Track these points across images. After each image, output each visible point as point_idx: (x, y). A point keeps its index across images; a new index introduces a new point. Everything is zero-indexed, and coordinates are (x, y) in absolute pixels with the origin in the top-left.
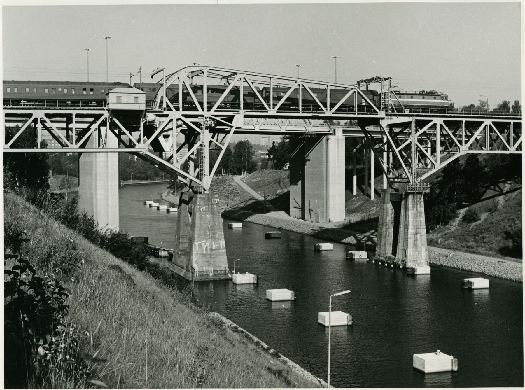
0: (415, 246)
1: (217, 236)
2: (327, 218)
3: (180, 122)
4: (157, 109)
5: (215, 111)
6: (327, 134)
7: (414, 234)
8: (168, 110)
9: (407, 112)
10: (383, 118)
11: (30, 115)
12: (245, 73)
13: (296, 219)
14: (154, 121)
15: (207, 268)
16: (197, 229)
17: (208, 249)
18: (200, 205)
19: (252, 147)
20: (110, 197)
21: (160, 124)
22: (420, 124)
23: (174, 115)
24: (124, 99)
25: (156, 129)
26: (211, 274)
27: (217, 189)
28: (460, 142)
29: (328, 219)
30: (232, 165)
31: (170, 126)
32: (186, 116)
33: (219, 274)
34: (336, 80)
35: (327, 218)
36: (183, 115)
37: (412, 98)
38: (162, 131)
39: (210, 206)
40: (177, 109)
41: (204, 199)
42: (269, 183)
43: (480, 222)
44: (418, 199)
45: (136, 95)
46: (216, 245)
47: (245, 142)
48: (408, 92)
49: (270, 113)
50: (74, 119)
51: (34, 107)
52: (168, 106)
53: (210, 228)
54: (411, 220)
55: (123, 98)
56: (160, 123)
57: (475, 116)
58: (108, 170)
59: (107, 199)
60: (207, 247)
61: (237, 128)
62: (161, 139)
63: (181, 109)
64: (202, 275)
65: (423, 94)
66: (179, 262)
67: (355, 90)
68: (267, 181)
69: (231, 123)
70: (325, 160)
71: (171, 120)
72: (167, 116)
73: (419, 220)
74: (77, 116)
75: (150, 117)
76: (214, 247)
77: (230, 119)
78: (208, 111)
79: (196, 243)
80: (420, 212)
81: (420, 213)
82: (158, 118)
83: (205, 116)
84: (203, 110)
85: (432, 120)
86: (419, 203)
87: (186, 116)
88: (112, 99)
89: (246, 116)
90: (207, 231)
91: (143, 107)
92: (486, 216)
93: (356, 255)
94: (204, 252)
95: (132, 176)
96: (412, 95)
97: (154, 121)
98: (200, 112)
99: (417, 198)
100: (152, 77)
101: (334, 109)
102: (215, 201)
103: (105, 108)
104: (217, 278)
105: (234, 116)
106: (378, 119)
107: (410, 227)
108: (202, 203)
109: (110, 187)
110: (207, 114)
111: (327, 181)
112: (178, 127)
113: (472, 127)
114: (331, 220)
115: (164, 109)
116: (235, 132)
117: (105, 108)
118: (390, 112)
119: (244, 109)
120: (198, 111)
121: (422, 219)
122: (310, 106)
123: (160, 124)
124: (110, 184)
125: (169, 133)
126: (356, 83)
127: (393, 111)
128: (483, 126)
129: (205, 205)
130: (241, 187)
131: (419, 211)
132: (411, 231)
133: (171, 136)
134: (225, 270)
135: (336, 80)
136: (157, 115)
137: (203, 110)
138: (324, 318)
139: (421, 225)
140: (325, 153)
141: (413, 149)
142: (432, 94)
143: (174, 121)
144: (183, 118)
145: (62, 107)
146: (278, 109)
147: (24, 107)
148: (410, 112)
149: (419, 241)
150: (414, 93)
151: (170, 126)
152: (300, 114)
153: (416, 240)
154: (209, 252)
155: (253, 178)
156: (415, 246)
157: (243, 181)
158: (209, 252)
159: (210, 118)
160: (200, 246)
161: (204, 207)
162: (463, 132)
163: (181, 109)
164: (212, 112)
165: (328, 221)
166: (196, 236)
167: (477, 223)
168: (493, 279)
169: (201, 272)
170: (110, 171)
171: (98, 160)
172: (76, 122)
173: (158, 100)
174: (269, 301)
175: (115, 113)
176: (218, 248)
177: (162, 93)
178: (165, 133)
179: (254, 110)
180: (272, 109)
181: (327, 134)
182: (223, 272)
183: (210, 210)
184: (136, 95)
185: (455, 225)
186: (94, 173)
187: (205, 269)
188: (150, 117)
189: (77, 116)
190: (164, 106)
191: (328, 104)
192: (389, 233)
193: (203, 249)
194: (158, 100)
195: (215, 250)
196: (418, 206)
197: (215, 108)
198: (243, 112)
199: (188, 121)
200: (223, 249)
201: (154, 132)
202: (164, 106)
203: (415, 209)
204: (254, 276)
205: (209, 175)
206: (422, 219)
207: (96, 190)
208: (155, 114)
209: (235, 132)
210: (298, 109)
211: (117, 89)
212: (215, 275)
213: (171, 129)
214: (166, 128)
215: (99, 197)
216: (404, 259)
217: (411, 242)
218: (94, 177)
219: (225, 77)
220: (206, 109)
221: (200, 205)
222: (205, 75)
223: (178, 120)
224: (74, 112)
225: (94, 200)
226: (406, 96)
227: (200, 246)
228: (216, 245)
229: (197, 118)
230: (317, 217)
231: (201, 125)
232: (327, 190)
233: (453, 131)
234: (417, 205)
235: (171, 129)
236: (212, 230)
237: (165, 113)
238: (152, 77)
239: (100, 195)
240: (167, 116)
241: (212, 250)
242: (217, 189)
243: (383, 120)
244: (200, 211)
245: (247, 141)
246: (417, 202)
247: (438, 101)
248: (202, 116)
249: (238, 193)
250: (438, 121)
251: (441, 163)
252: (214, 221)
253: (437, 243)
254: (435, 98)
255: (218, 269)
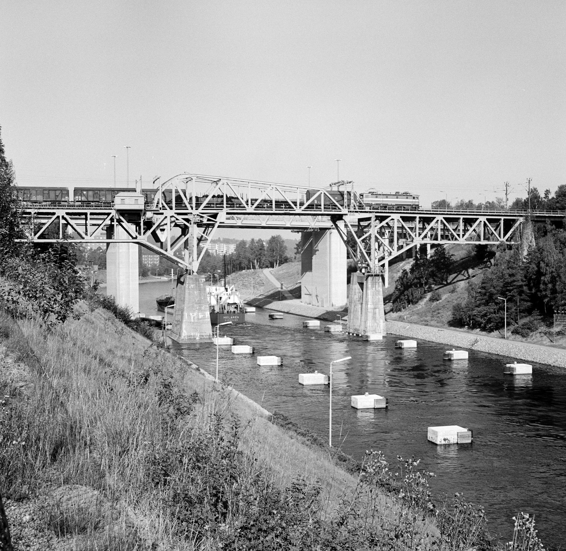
0: (374, 318)
1: (203, 308)
2: (330, 302)
3: (173, 219)
4: (155, 209)
5: (202, 209)
6: (330, 229)
7: (373, 309)
8: (163, 209)
9: (367, 209)
10: (347, 214)
11: (54, 214)
12: (227, 178)
13: (306, 305)
14: (152, 217)
15: (194, 333)
16: (186, 302)
17: (195, 318)
18: (189, 284)
19: (283, 241)
20: (131, 283)
21: (157, 220)
22: (382, 219)
23: (168, 213)
24: (127, 201)
25: (154, 224)
26: (197, 338)
27: (247, 281)
28: (459, 235)
29: (331, 303)
30: (264, 259)
31: (165, 222)
32: (178, 214)
33: (204, 339)
34: (309, 184)
35: (330, 302)
36: (175, 213)
37: (387, 197)
38: (159, 226)
39: (197, 284)
40: (171, 208)
41: (192, 279)
42: (293, 274)
43: (440, 301)
44: (377, 281)
45: (137, 198)
46: (202, 316)
47: (276, 237)
48: (384, 193)
49: (248, 211)
50: (89, 216)
51: (94, 207)
52: (163, 206)
53: (197, 302)
54: (370, 297)
55: (126, 200)
56: (157, 220)
57: (512, 214)
58: (129, 259)
59: (129, 284)
60: (194, 317)
61: (220, 223)
62: (158, 232)
63: (174, 208)
64: (190, 339)
65: (397, 195)
66: (175, 330)
67: (322, 192)
68: (291, 273)
69: (216, 219)
70: (328, 251)
71: (166, 217)
72: (162, 214)
73: (377, 297)
74: (91, 214)
75: (149, 215)
76: (201, 316)
77: (215, 216)
78: (196, 209)
79: (186, 314)
80: (378, 291)
81: (379, 291)
82: (155, 215)
83: (194, 213)
84: (192, 209)
85: (390, 216)
86: (377, 284)
87: (178, 214)
88: (117, 200)
89: (228, 213)
90: (194, 304)
91: (142, 207)
92: (447, 297)
93: (332, 328)
94: (192, 321)
95: (179, 271)
96: (387, 196)
97: (152, 217)
98: (190, 211)
99: (375, 280)
100: (154, 182)
101: (303, 208)
102: (202, 281)
103: (112, 208)
104: (203, 341)
105: (218, 213)
106: (342, 215)
107: (369, 303)
108: (191, 282)
109: (131, 274)
110: (195, 212)
111: (330, 270)
112: (171, 222)
113: (469, 222)
114: (334, 304)
115: (160, 209)
116: (219, 227)
117: (112, 208)
118: (352, 209)
119: (227, 207)
120: (188, 209)
121: (380, 297)
122: (282, 205)
123: (157, 220)
124: (131, 271)
125: (165, 227)
126: (329, 186)
127: (355, 209)
128: (478, 222)
129: (193, 284)
130: (267, 278)
131: (377, 290)
132: (370, 306)
133: (166, 230)
134: (210, 335)
135: (309, 184)
136: (154, 213)
137: (192, 209)
138: (435, 433)
139: (379, 302)
140: (328, 245)
141: (373, 239)
142: (406, 195)
143: (168, 218)
144: (176, 216)
145: (106, 208)
146: (256, 207)
147: (68, 208)
148: (370, 209)
149: (377, 315)
150: (390, 194)
151: (165, 222)
152: (274, 212)
153: (375, 313)
154: (196, 321)
155: (281, 270)
156: (374, 318)
157: (271, 273)
158: (196, 321)
159: (198, 215)
160: (189, 316)
161: (192, 286)
162: (418, 225)
163: (174, 208)
164: (200, 210)
165: (331, 305)
166: (185, 308)
167: (438, 302)
168: (472, 353)
169: (189, 336)
170: (131, 261)
171: (120, 251)
172: (91, 219)
173: (155, 202)
174: (355, 409)
175: (122, 212)
176: (204, 318)
177: (159, 196)
178: (161, 228)
179: (235, 208)
180: (250, 207)
181: (330, 229)
182: (207, 337)
183: (198, 288)
184: (137, 198)
185: (422, 304)
186: (117, 263)
187: (192, 334)
188: (149, 215)
189: (91, 214)
190: (160, 206)
191: (298, 204)
192: (356, 309)
193: (191, 318)
194: (155, 202)
195: (201, 319)
196: (377, 286)
197: (202, 207)
198: (226, 210)
199: (180, 217)
200: (208, 318)
201: (152, 227)
202: (160, 206)
203: (374, 288)
204: (324, 376)
205: (197, 260)
206: (380, 297)
207: (119, 276)
208: (153, 212)
209: (219, 227)
210: (271, 207)
211: (121, 194)
212: (201, 339)
213: (166, 224)
214: (162, 224)
215: (121, 282)
216: (365, 329)
217: (370, 315)
218: (117, 265)
219: (215, 182)
220: (194, 208)
221: (189, 284)
222: (194, 180)
223: (171, 217)
224: (88, 212)
225: (118, 285)
226: (382, 196)
227: (189, 316)
228: (202, 316)
229: (187, 215)
230: (322, 301)
231: (190, 221)
232: (330, 278)
233: (495, 228)
234: (376, 285)
235: (166, 224)
236: (199, 303)
237: (161, 211)
238: (154, 182)
239: (122, 280)
240: (162, 214)
241: (198, 319)
242: (247, 281)
243: (346, 216)
244: (189, 288)
245: (279, 236)
246: (376, 282)
247: (410, 201)
248: (191, 213)
249: (263, 283)
250: (397, 217)
251: (398, 251)
252: (200, 296)
253: (404, 319)
254: (407, 198)
255: (203, 335)
